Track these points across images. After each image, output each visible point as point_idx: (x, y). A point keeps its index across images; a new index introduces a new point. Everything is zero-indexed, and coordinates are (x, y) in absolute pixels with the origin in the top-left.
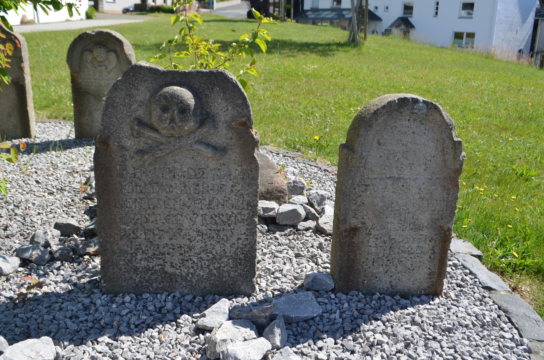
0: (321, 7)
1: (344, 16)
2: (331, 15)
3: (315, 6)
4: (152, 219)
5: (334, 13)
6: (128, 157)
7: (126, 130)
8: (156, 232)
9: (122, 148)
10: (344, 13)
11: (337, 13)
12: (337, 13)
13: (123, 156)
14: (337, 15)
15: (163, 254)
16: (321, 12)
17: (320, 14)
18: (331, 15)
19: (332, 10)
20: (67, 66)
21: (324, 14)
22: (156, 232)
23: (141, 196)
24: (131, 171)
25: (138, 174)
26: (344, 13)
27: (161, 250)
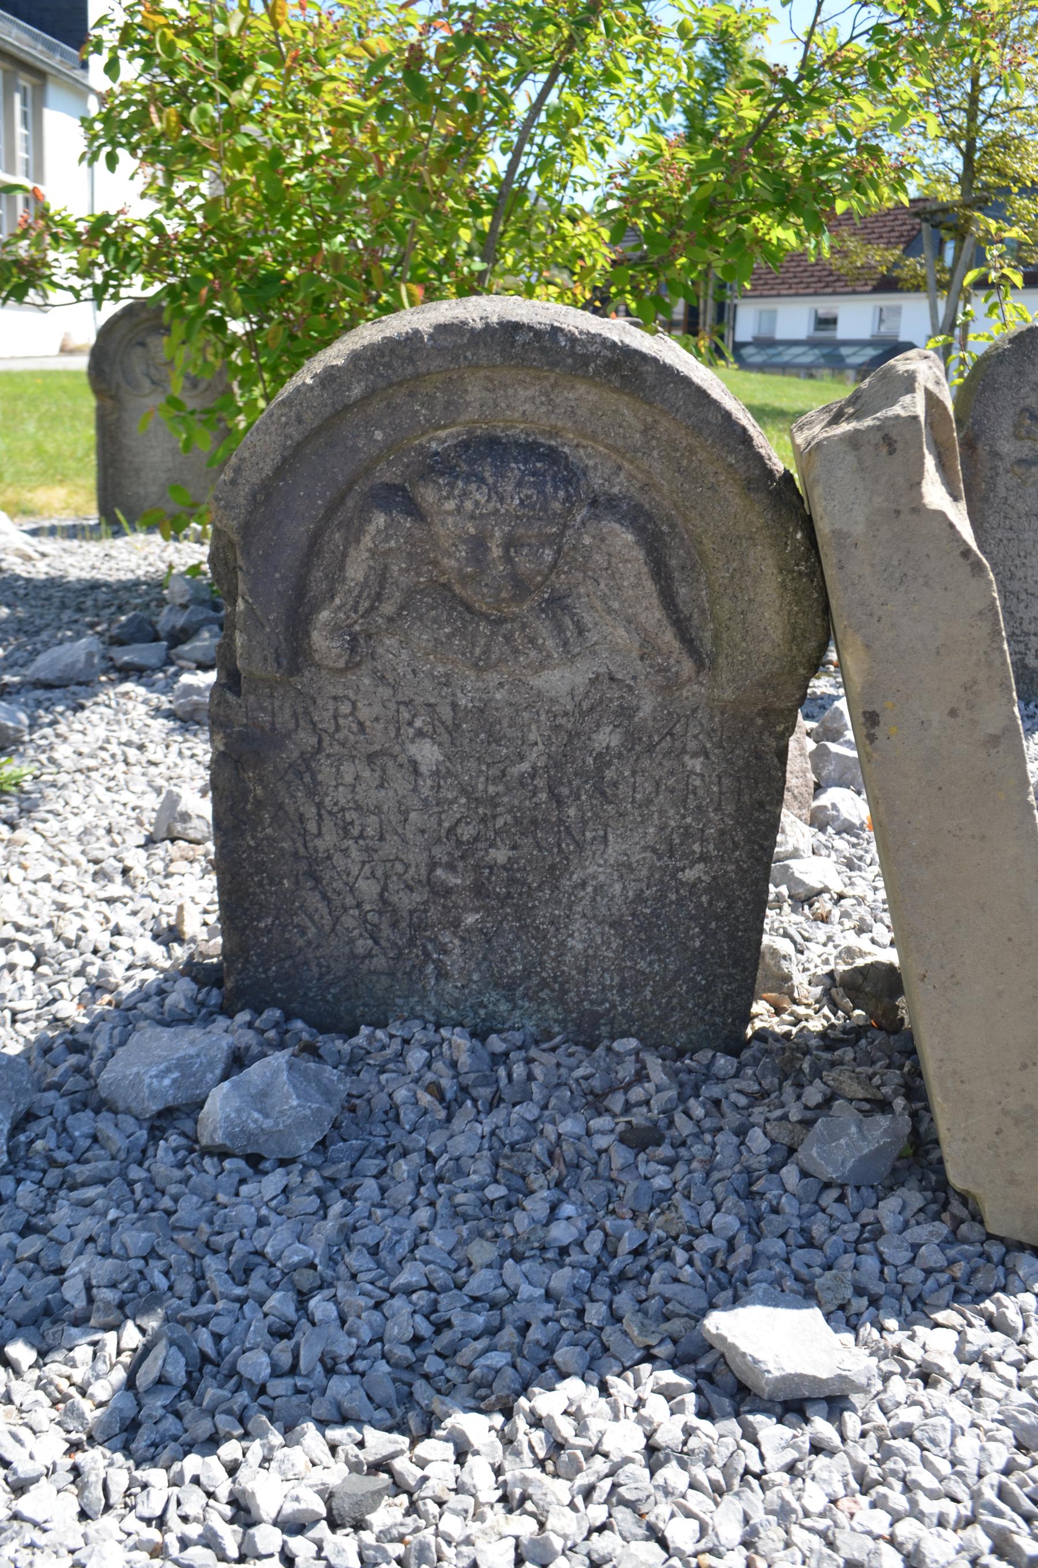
0: (780, 335)
1: (841, 359)
2: (809, 357)
3: (765, 333)
4: (1020, 573)
5: (817, 351)
6: (1001, 471)
7: (1006, 426)
8: (1023, 596)
9: (995, 454)
10: (844, 351)
11: (826, 351)
12: (826, 351)
13: (994, 468)
14: (824, 356)
15: (1027, 634)
16: (780, 349)
17: (780, 354)
18: (809, 357)
19: (811, 343)
20: (93, 459)
21: (788, 355)
22: (1023, 596)
23: (1010, 535)
24: (1002, 493)
25: (1011, 500)
26: (844, 351)
27: (1026, 627)
